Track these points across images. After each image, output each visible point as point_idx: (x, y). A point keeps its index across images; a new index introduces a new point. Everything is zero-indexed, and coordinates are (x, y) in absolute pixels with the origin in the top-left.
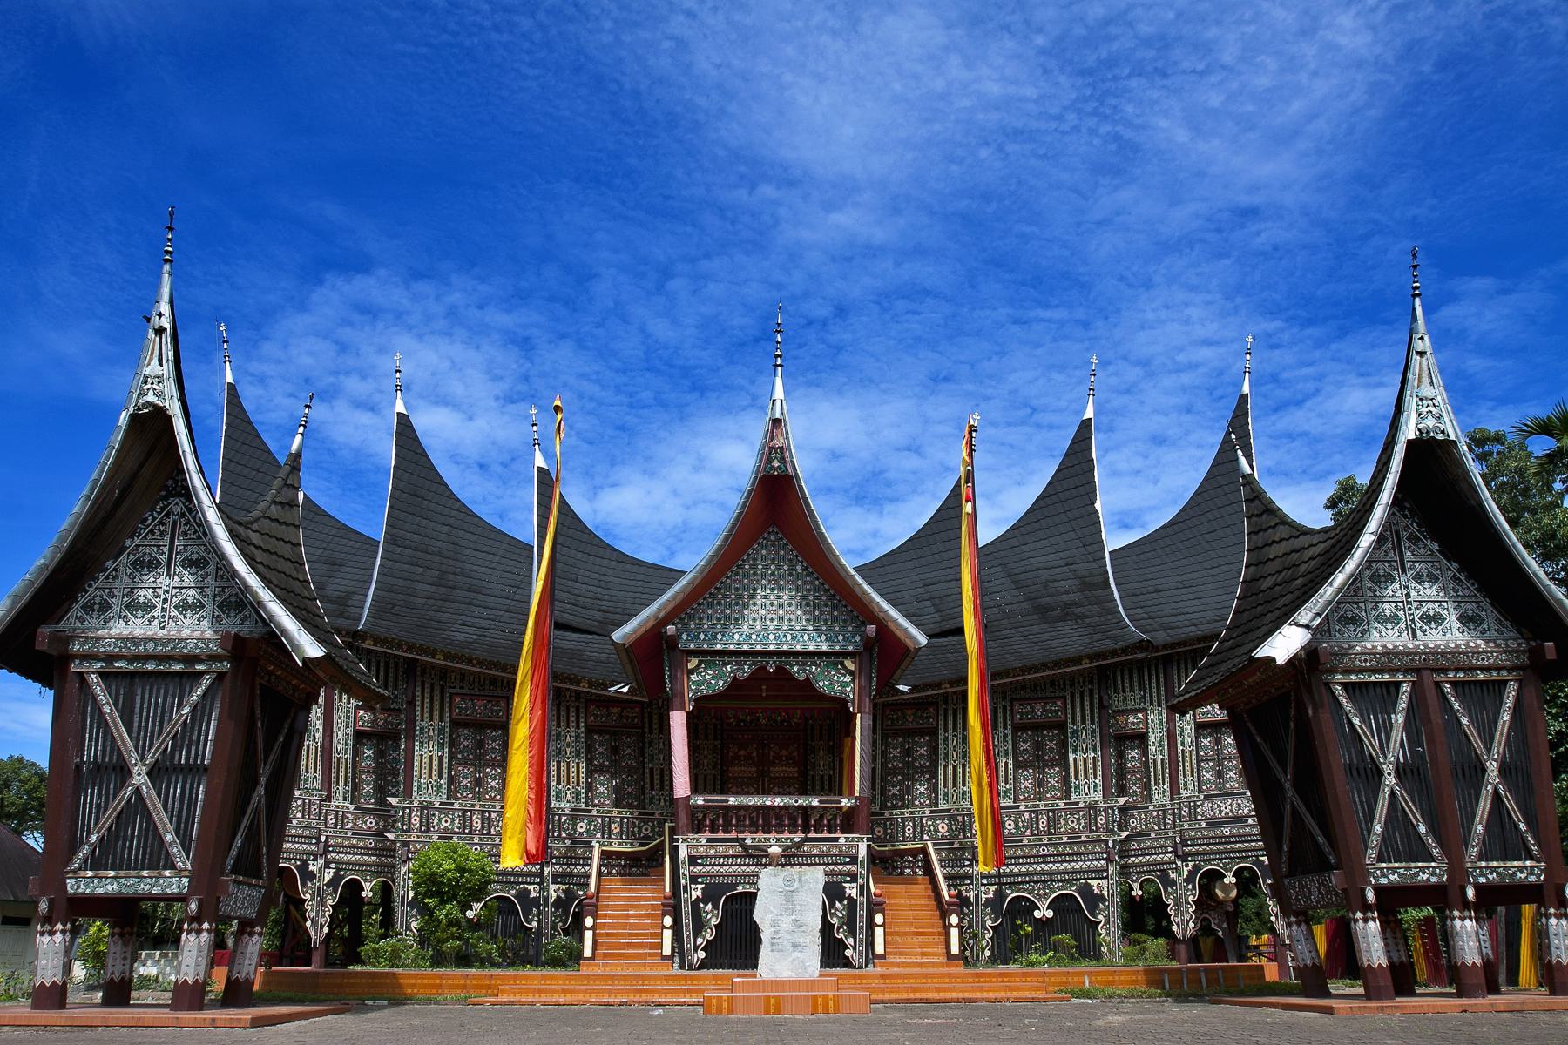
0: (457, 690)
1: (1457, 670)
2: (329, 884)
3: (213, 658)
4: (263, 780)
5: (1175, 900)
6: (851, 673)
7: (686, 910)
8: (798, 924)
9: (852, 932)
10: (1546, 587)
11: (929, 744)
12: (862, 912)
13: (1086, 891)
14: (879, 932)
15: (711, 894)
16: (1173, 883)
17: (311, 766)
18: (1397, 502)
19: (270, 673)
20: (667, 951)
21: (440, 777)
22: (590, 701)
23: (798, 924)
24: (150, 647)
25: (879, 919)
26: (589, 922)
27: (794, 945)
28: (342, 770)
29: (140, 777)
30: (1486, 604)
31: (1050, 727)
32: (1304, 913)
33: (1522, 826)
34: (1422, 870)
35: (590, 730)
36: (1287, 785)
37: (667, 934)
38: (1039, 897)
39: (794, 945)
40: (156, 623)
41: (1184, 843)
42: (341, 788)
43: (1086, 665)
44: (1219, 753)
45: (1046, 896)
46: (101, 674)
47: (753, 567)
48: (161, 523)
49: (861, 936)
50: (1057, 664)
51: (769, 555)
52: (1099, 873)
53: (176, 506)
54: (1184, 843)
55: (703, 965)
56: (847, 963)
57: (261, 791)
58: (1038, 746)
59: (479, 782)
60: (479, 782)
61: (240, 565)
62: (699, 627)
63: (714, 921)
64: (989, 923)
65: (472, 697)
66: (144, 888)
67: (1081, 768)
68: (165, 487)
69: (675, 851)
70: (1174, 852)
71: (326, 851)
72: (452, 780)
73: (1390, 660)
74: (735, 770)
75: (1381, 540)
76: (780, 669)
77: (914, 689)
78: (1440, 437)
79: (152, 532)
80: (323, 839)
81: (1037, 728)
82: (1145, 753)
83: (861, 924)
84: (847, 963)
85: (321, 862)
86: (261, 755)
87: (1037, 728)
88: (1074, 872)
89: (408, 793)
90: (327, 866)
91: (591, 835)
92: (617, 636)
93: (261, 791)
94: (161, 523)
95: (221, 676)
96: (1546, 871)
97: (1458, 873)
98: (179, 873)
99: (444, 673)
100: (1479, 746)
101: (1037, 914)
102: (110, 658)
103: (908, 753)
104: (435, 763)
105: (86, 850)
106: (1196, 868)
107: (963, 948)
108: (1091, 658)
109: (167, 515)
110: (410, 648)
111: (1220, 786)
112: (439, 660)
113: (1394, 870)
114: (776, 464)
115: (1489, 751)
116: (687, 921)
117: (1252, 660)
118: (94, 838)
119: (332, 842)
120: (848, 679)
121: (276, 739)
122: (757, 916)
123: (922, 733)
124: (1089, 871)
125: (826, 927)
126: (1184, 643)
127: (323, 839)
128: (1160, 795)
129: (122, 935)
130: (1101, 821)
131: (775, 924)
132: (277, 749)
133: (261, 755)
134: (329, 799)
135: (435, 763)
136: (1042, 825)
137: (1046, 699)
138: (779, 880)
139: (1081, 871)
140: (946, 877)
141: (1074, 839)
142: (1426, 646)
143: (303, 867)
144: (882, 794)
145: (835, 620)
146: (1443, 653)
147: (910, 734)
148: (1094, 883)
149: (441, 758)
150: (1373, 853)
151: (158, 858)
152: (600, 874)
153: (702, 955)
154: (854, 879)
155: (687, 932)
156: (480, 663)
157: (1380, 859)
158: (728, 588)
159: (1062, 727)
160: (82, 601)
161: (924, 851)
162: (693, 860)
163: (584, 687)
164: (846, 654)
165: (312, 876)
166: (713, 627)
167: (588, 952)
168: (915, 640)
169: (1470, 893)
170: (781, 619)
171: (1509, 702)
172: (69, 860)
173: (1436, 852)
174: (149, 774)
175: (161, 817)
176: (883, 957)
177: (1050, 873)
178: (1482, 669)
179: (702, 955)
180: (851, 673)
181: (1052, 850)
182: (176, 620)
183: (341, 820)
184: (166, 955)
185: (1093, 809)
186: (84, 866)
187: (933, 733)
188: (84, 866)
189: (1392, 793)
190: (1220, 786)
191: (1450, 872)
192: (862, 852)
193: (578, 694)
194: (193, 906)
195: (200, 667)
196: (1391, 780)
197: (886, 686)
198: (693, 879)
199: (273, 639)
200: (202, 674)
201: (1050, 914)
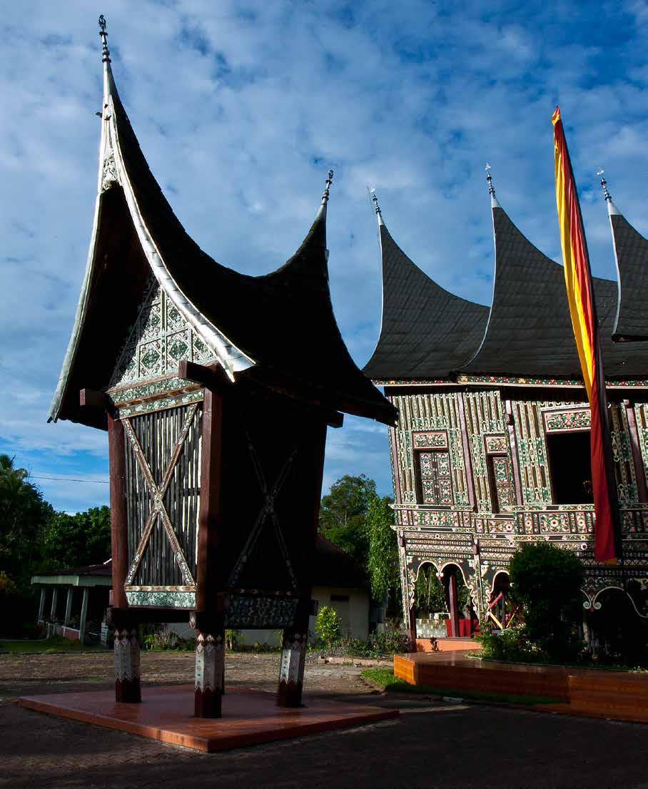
2: (485, 577)
21: (544, 485)
71: (478, 552)
80: (476, 542)
85: (477, 558)
104: (538, 473)
111: (438, 501)
127: (476, 542)
135: (538, 473)
149: (542, 468)
151: (173, 577)
165: (471, 571)
183: (486, 527)
184: (425, 622)
190: (438, 501)
201: (598, 606)
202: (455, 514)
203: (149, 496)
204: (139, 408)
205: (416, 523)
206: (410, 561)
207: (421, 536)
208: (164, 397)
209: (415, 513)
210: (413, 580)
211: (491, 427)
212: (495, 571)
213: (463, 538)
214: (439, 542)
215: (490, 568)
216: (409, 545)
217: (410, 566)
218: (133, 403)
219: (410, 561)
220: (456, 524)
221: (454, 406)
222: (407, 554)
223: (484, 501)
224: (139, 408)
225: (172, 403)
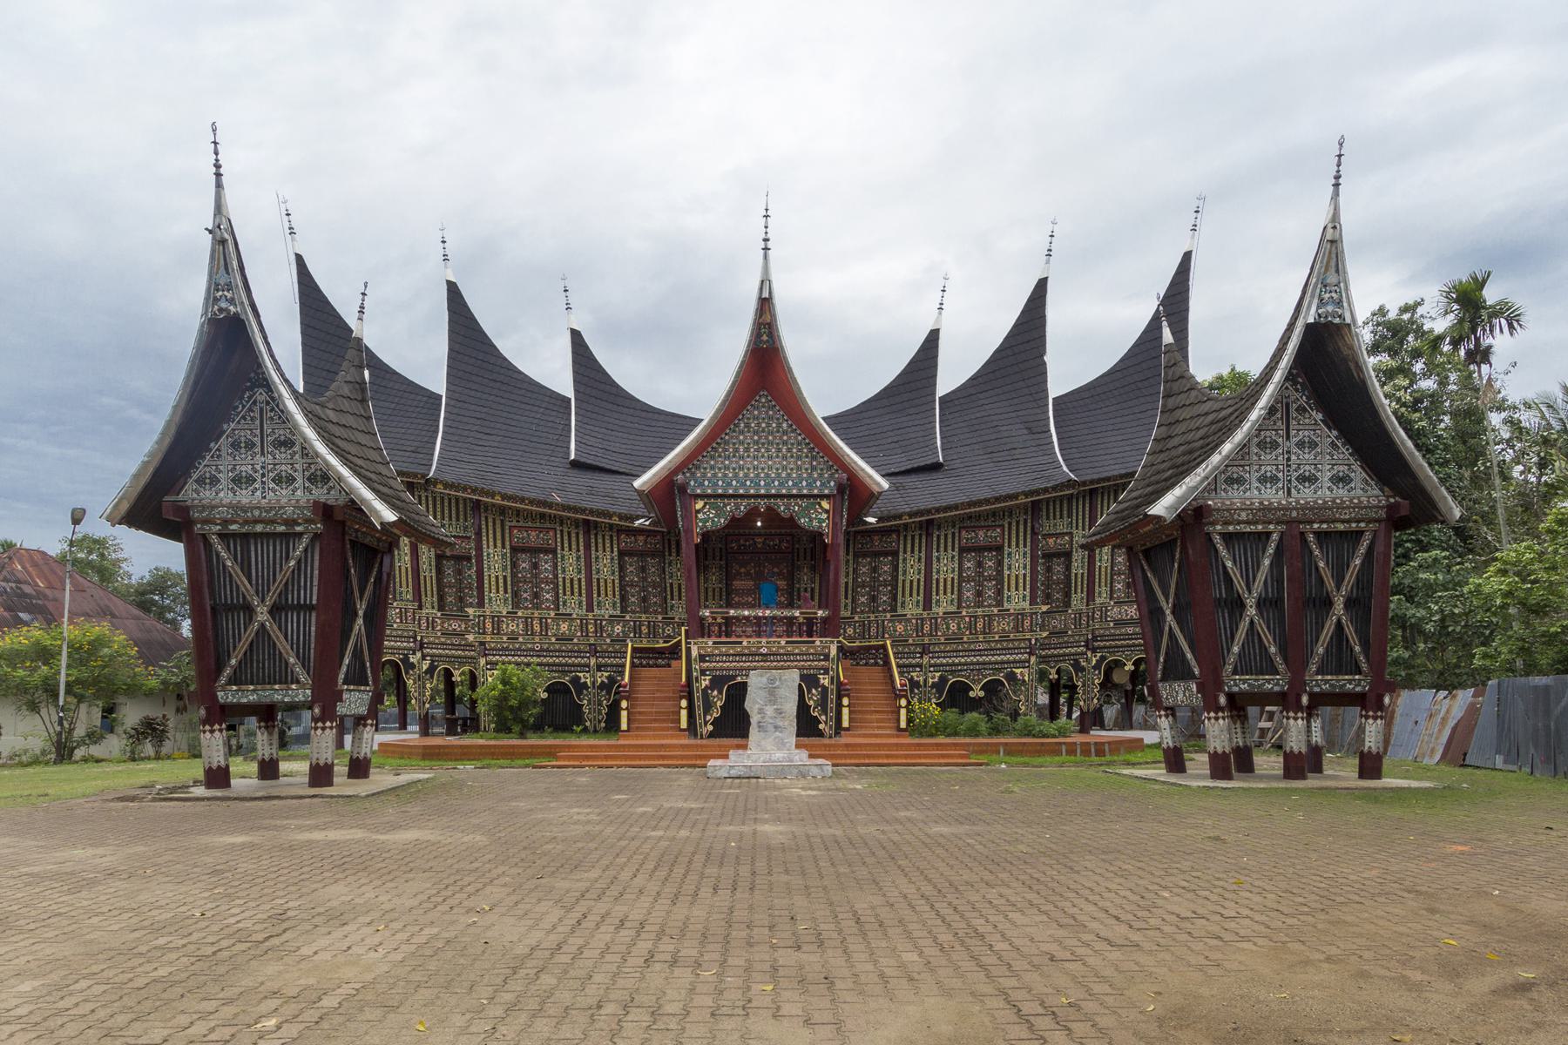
1: (1322, 522)
2: (426, 672)
3: (308, 521)
4: (361, 613)
6: (827, 512)
7: (697, 695)
8: (779, 712)
10: (1411, 454)
11: (892, 563)
12: (832, 697)
13: (1011, 677)
14: (845, 711)
15: (717, 682)
16: (1083, 669)
18: (1290, 377)
19: (357, 531)
20: (684, 724)
22: (620, 530)
23: (779, 712)
24: (257, 513)
25: (845, 701)
26: (624, 704)
27: (776, 727)
29: (262, 615)
30: (1356, 466)
31: (990, 549)
32: (1172, 709)
33: (1357, 649)
34: (1268, 681)
35: (622, 554)
36: (1168, 612)
37: (684, 713)
38: (974, 681)
39: (776, 727)
40: (258, 493)
41: (1095, 639)
42: (430, 599)
43: (1022, 500)
44: (536, 576)
45: (979, 681)
46: (220, 535)
47: (748, 426)
48: (251, 410)
50: (997, 499)
51: (762, 413)
52: (1023, 664)
53: (260, 395)
54: (1095, 639)
55: (711, 735)
56: (820, 734)
57: (360, 621)
58: (980, 564)
59: (536, 595)
60: (536, 595)
61: (321, 448)
62: (704, 475)
63: (719, 704)
65: (527, 529)
66: (278, 697)
67: (1013, 582)
68: (249, 380)
69: (689, 650)
70: (1086, 646)
71: (422, 647)
72: (516, 594)
73: (1265, 512)
74: (737, 584)
75: (1271, 411)
76: (769, 508)
77: (880, 519)
78: (1337, 321)
79: (244, 418)
81: (980, 549)
82: (1068, 568)
83: (832, 705)
84: (820, 734)
85: (419, 655)
86: (357, 594)
87: (980, 549)
88: (1003, 662)
89: (481, 604)
90: (424, 657)
91: (626, 636)
92: (637, 483)
93: (360, 621)
94: (251, 410)
95: (316, 537)
96: (1371, 684)
97: (1298, 684)
98: (303, 686)
99: (502, 511)
100: (1330, 583)
101: (972, 694)
102: (226, 522)
103: (874, 570)
105: (228, 671)
106: (1103, 658)
107: (909, 721)
108: (1026, 494)
109: (255, 403)
110: (474, 491)
112: (498, 500)
113: (1245, 681)
114: (765, 338)
115: (1338, 588)
116: (699, 703)
117: (1146, 515)
118: (233, 662)
120: (824, 516)
121: (367, 581)
122: (748, 705)
123: (886, 554)
124: (1015, 662)
125: (803, 708)
126: (1108, 479)
128: (1078, 600)
129: (267, 727)
130: (1027, 624)
131: (761, 711)
132: (370, 587)
133: (357, 594)
134: (420, 607)
136: (980, 625)
137: (988, 528)
138: (764, 680)
139: (1008, 662)
140: (898, 666)
141: (1005, 637)
142: (1297, 502)
143: (406, 660)
144: (853, 601)
145: (814, 468)
146: (1311, 509)
147: (877, 554)
148: (1018, 671)
150: (1229, 668)
152: (633, 665)
153: (710, 728)
154: (826, 672)
155: (699, 712)
156: (532, 502)
157: (1235, 672)
158: (727, 443)
159: (999, 549)
160: (195, 477)
161: (884, 647)
162: (702, 658)
163: (615, 520)
164: (822, 497)
165: (412, 666)
166: (715, 475)
167: (624, 726)
168: (878, 484)
169: (1305, 700)
170: (770, 468)
171: (1362, 550)
172: (216, 679)
173: (1281, 668)
174: (271, 612)
175: (283, 645)
176: (847, 729)
177: (984, 663)
178: (1343, 521)
179: (710, 728)
180: (827, 512)
181: (986, 646)
182: (274, 491)
185: (1019, 616)
186: (230, 682)
187: (895, 554)
188: (230, 682)
189: (1252, 622)
191: (1290, 683)
192: (834, 652)
193: (611, 526)
194: (317, 711)
195: (299, 529)
196: (1252, 611)
197: (856, 518)
198: (703, 672)
199: (355, 508)
200: (301, 534)
201: (982, 694)
204: (234, 527)
224: (234, 527)
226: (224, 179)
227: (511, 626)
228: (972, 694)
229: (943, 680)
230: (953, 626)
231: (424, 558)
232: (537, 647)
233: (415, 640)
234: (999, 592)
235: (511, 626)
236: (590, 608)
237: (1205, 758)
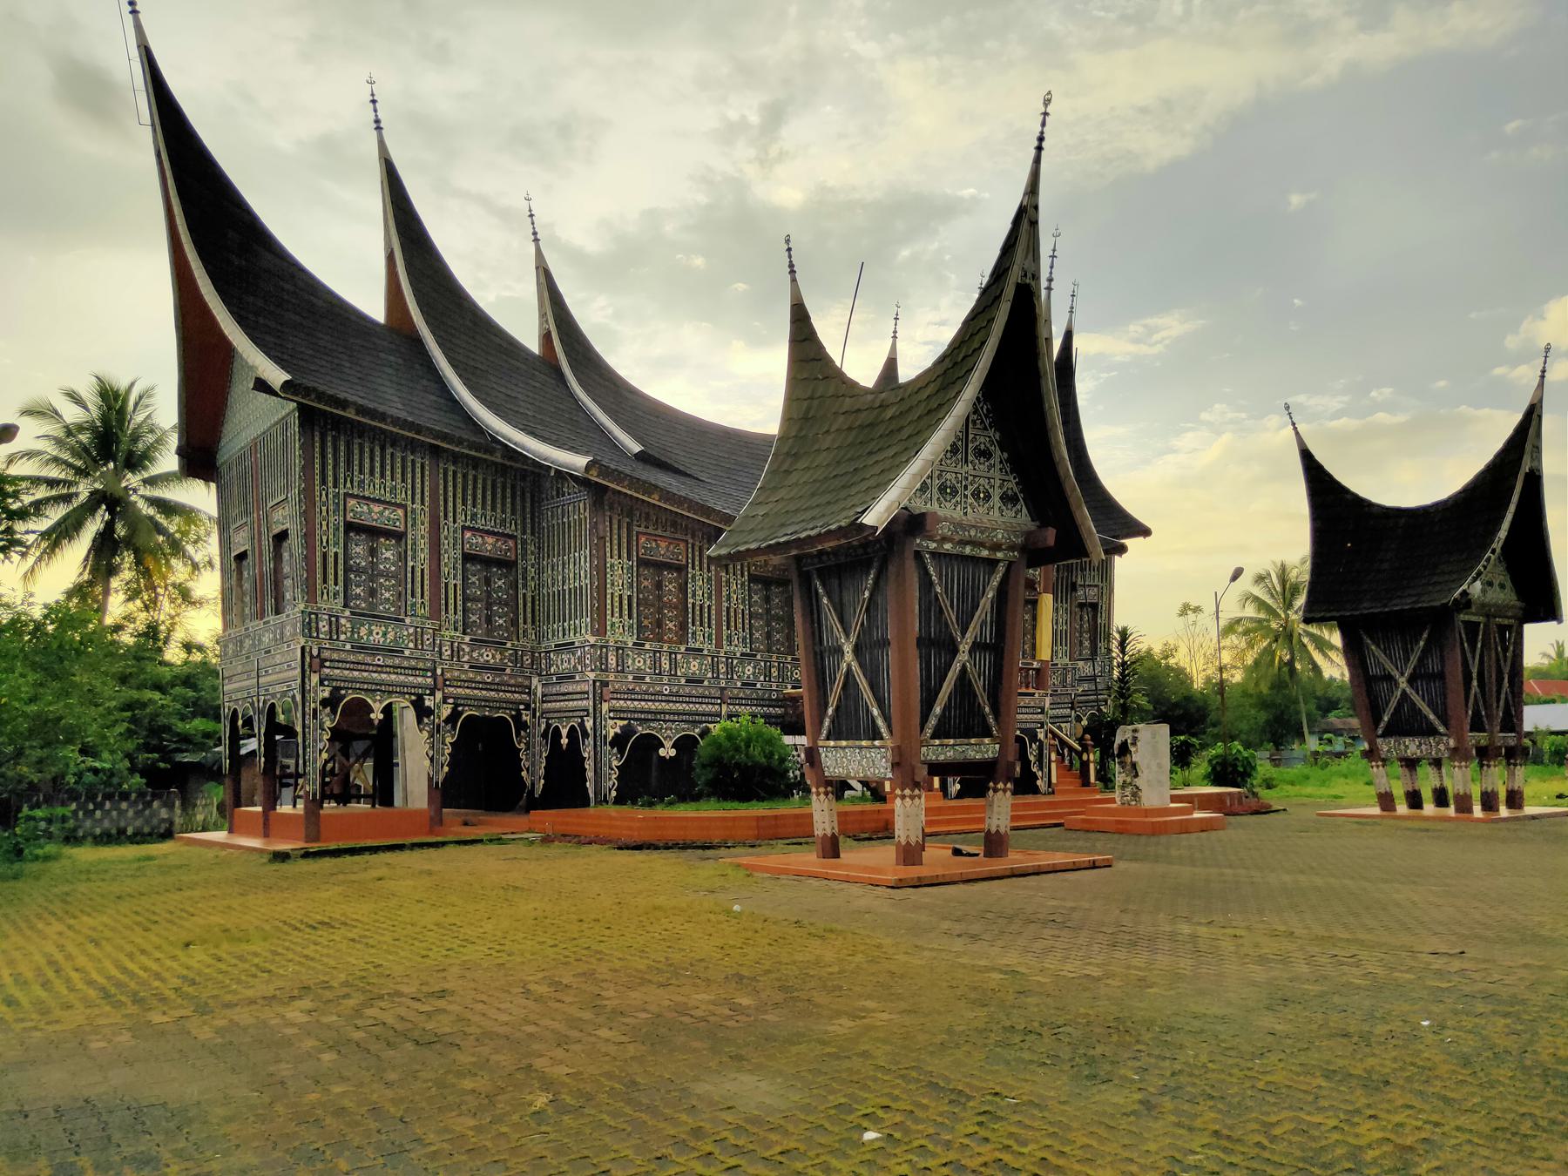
0: (642, 529)
2: (447, 721)
5: (527, 744)
9: (1041, 768)
17: (451, 592)
28: (454, 598)
29: (1403, 683)
44: (660, 598)
49: (1046, 770)
64: (615, 763)
80: (439, 672)
85: (439, 695)
101: (662, 752)
119: (448, 675)
159: (680, 569)
201: (673, 753)
202: (411, 630)
203: (839, 651)
204: (948, 546)
205: (343, 637)
206: (326, 694)
207: (352, 658)
208: (981, 545)
209: (343, 621)
210: (328, 724)
211: (474, 516)
212: (461, 713)
213: (421, 665)
214: (380, 668)
215: (454, 710)
216: (327, 671)
217: (324, 703)
218: (944, 539)
219: (326, 694)
220: (411, 645)
221: (475, 488)
222: (321, 684)
223: (451, 617)
224: (948, 546)
225: (985, 553)
226: (797, 276)
227: (638, 662)
228: (662, 752)
229: (627, 732)
230: (749, 670)
231: (424, 556)
232: (666, 690)
233: (434, 676)
234: (683, 627)
235: (638, 662)
236: (719, 645)
237: (818, 832)
